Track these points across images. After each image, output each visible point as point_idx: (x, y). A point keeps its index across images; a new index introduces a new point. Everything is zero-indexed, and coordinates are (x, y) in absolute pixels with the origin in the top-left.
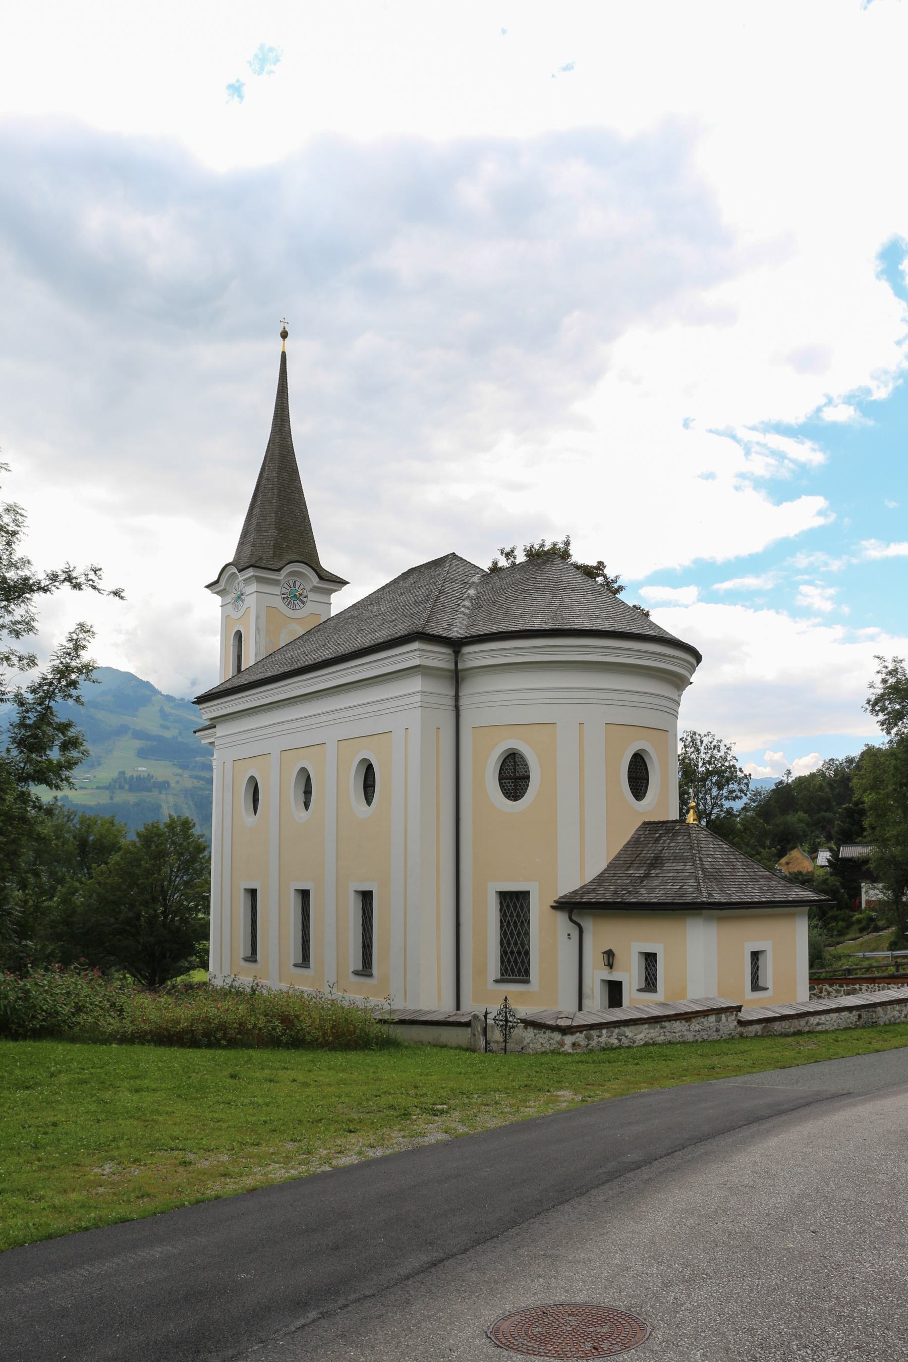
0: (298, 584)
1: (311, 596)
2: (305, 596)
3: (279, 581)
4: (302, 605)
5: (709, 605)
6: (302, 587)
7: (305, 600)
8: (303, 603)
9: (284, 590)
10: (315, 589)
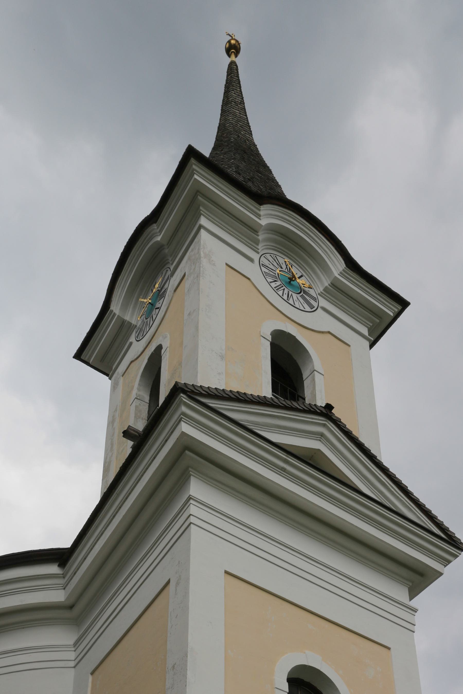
8: (311, 306)
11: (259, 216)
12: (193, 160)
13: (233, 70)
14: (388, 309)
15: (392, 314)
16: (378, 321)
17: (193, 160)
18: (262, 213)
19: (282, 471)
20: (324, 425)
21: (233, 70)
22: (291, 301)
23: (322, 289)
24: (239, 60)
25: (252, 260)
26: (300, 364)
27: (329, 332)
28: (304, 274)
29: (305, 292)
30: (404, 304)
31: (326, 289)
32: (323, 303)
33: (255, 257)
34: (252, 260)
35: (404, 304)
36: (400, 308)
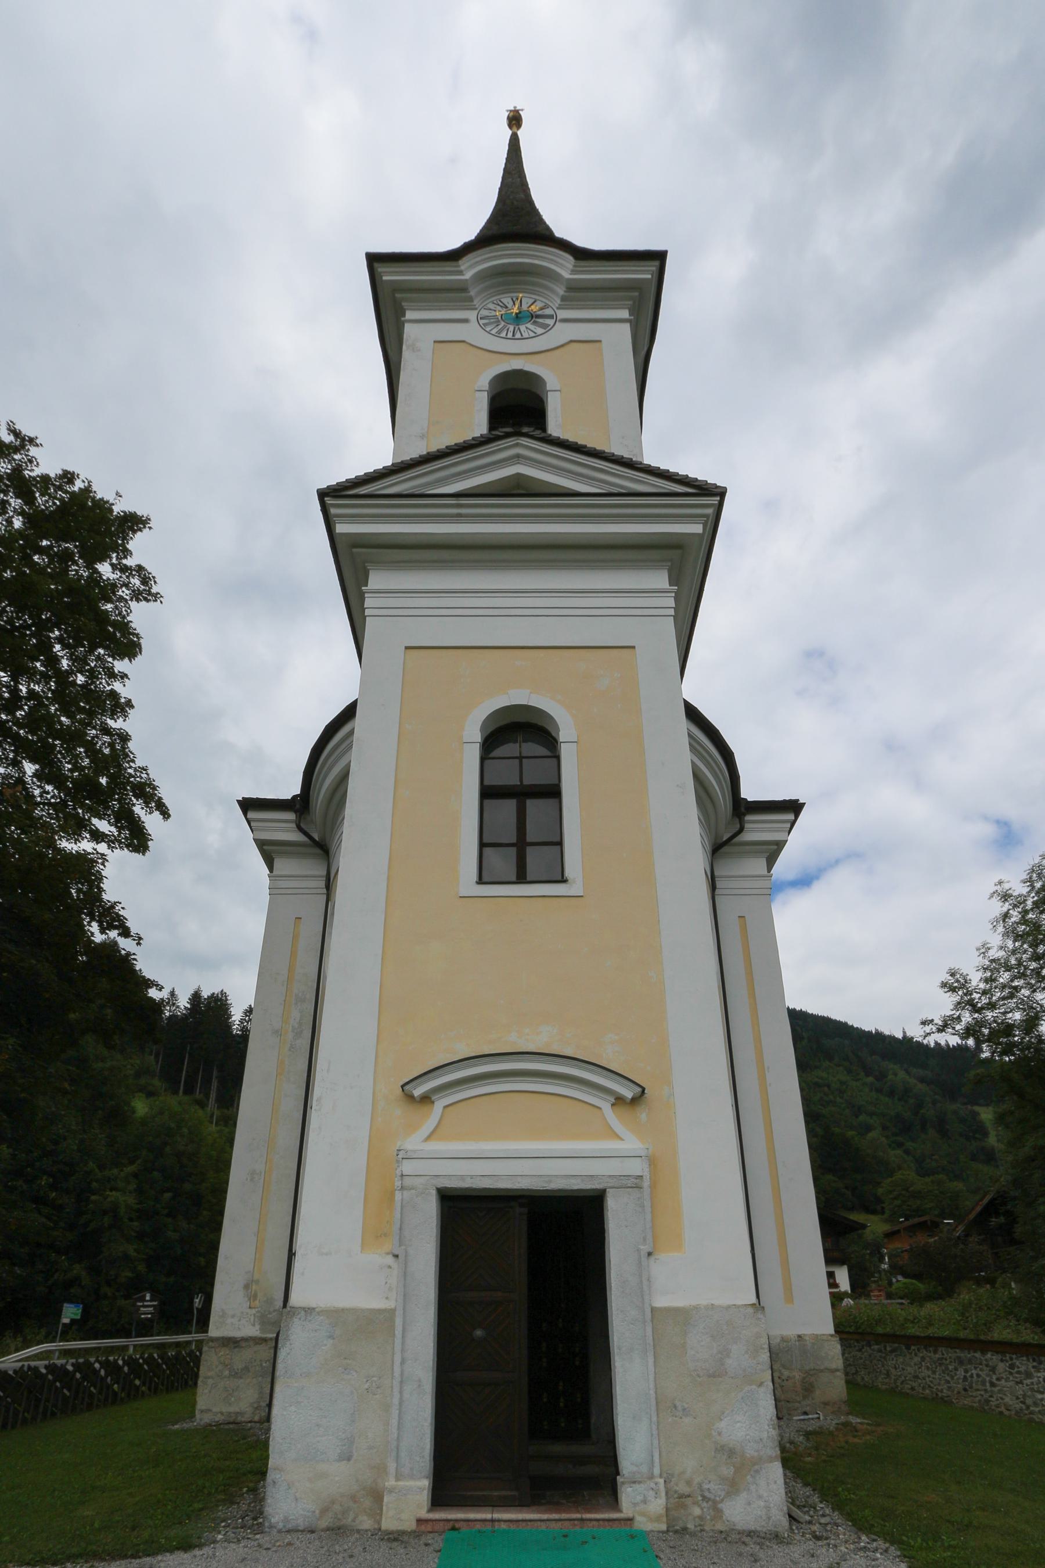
2: (551, 317)
5: (843, 1020)
8: (544, 326)
11: (461, 273)
12: (376, 265)
13: (514, 146)
14: (644, 273)
15: (649, 276)
16: (636, 294)
17: (376, 265)
18: (462, 268)
19: (458, 518)
20: (517, 445)
21: (514, 146)
22: (525, 335)
23: (559, 301)
24: (519, 133)
25: (466, 321)
26: (538, 392)
27: (572, 341)
28: (537, 297)
29: (538, 316)
30: (659, 257)
31: (564, 299)
32: (562, 314)
33: (472, 315)
34: (466, 321)
35: (659, 257)
36: (657, 263)
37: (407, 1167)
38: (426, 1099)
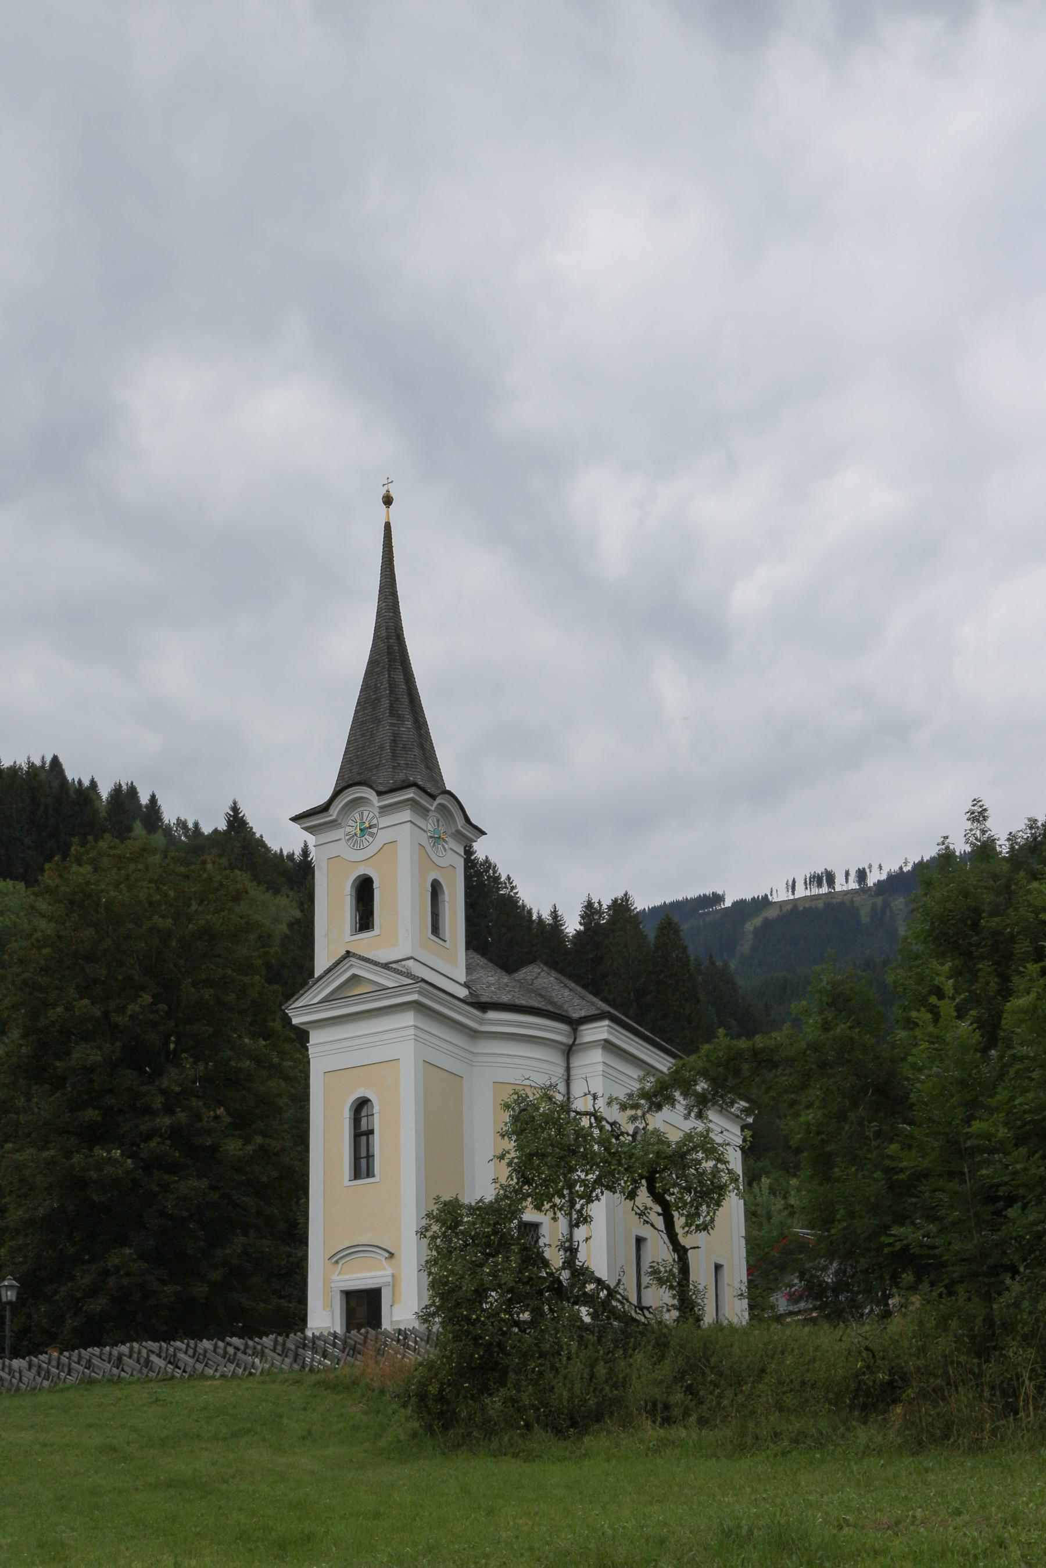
0: (366, 813)
1: (384, 821)
3: (428, 810)
4: (371, 839)
6: (371, 815)
7: (446, 846)
8: (372, 835)
9: (348, 829)
10: (384, 810)
37: (333, 1285)
38: (337, 1262)
